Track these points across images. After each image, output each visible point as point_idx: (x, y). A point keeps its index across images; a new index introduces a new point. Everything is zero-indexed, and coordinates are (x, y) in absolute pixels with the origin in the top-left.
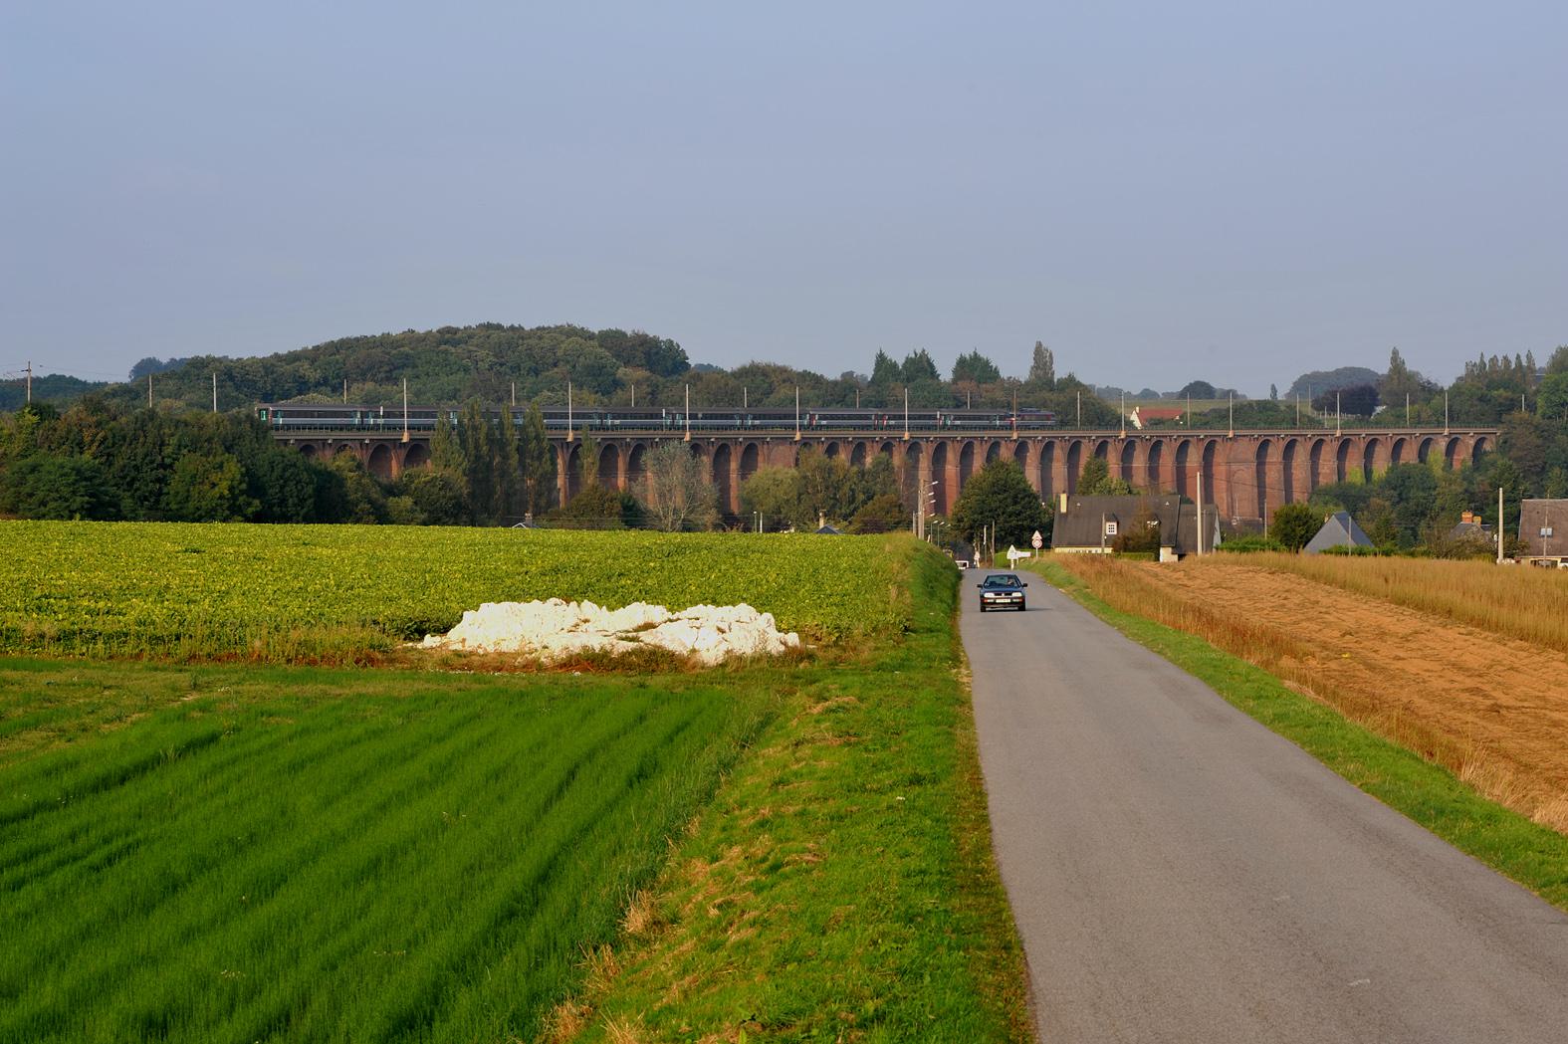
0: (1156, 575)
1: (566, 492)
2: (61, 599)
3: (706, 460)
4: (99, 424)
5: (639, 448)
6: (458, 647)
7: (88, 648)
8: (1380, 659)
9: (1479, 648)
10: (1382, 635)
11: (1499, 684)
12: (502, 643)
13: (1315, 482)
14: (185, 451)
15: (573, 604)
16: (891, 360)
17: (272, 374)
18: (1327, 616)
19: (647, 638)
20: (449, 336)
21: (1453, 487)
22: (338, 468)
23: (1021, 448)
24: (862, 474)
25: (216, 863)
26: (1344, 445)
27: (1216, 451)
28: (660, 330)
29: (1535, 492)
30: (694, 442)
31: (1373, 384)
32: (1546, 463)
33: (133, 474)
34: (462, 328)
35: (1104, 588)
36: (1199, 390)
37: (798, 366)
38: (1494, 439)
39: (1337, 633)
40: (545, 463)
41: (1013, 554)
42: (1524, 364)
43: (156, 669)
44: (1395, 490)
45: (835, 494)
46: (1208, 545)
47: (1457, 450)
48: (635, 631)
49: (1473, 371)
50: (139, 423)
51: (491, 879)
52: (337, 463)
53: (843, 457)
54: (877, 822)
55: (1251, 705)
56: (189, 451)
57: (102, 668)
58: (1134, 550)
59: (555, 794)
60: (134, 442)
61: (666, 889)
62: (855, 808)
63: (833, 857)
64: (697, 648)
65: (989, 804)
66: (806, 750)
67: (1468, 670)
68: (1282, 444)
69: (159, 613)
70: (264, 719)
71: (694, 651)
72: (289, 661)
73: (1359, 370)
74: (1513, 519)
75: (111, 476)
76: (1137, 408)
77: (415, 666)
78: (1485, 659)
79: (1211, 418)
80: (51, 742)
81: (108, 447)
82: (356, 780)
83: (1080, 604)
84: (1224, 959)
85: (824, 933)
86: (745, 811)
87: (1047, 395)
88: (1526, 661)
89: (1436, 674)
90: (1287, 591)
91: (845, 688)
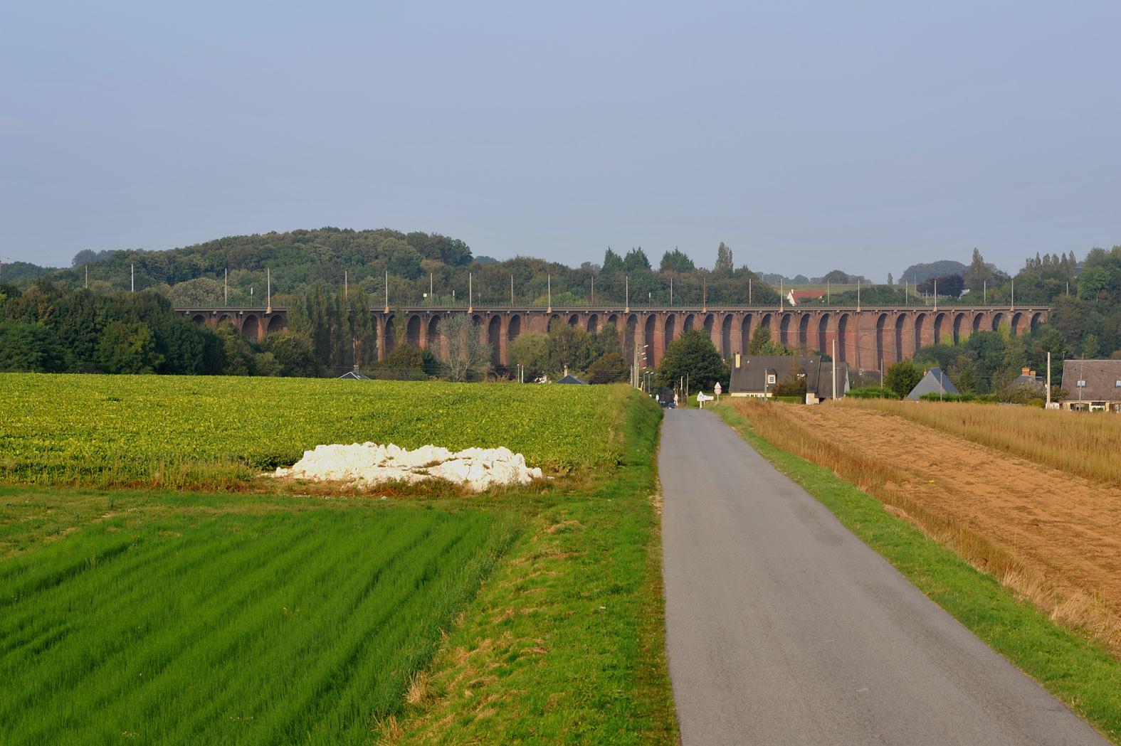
0: (801, 417)
1: (383, 349)
2: (19, 438)
3: (484, 328)
4: (49, 300)
5: (436, 318)
6: (300, 476)
7: (37, 477)
8: (956, 484)
9: (1028, 475)
10: (959, 464)
11: (1040, 503)
12: (332, 474)
13: (918, 344)
14: (111, 320)
15: (382, 446)
16: (616, 255)
17: (174, 263)
18: (920, 450)
19: (434, 472)
20: (300, 236)
21: (1016, 349)
22: (221, 332)
23: (709, 320)
24: (595, 337)
25: (122, 648)
26: (940, 318)
27: (848, 322)
28: (452, 233)
29: (1075, 353)
30: (476, 314)
31: (961, 274)
32: (1083, 331)
33: (74, 335)
34: (310, 230)
35: (763, 427)
36: (837, 277)
37: (550, 259)
38: (1046, 314)
39: (927, 464)
40: (369, 328)
41: (701, 397)
42: (1068, 257)
43: (85, 493)
44: (975, 350)
45: (576, 352)
46: (841, 392)
47: (1019, 322)
48: (425, 467)
49: (1031, 265)
50: (78, 299)
51: (315, 660)
52: (220, 329)
53: (582, 325)
54: (586, 623)
55: (858, 527)
56: (114, 320)
57: (47, 492)
58: (788, 394)
59: (363, 593)
60: (75, 313)
61: (439, 669)
62: (571, 612)
63: (554, 651)
64: (469, 479)
65: (666, 609)
66: (538, 564)
67: (1018, 492)
68: (895, 317)
69: (88, 449)
70: (160, 533)
71: (467, 481)
72: (179, 487)
73: (951, 262)
74: (1057, 372)
75: (58, 338)
76: (792, 290)
77: (269, 491)
78: (1031, 484)
79: (846, 298)
80: (9, 550)
81: (55, 317)
82: (223, 583)
83: (745, 440)
84: (818, 740)
85: (542, 715)
86: (496, 610)
87: (727, 280)
88: (1060, 485)
89: (995, 496)
90: (894, 430)
91: (571, 514)
